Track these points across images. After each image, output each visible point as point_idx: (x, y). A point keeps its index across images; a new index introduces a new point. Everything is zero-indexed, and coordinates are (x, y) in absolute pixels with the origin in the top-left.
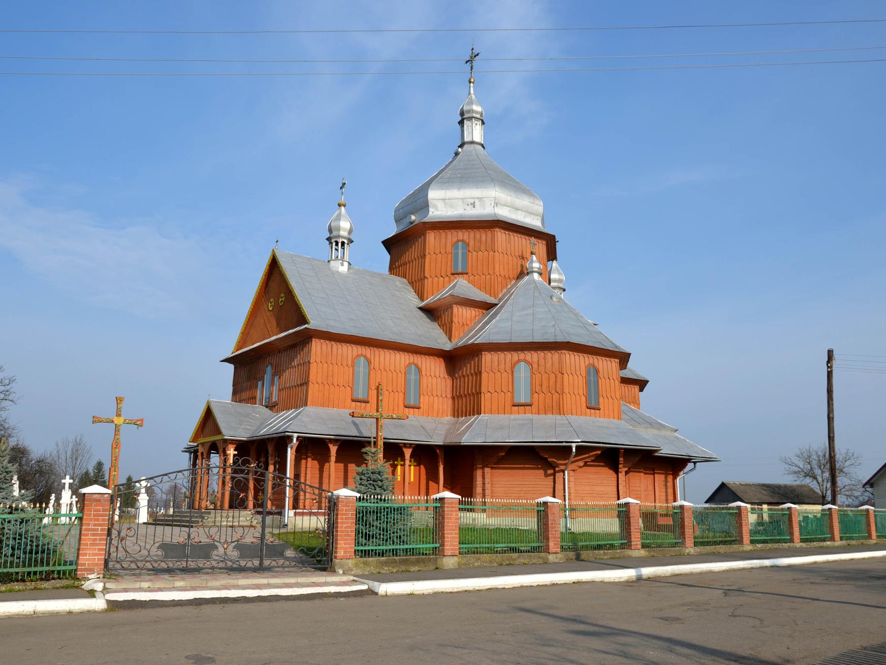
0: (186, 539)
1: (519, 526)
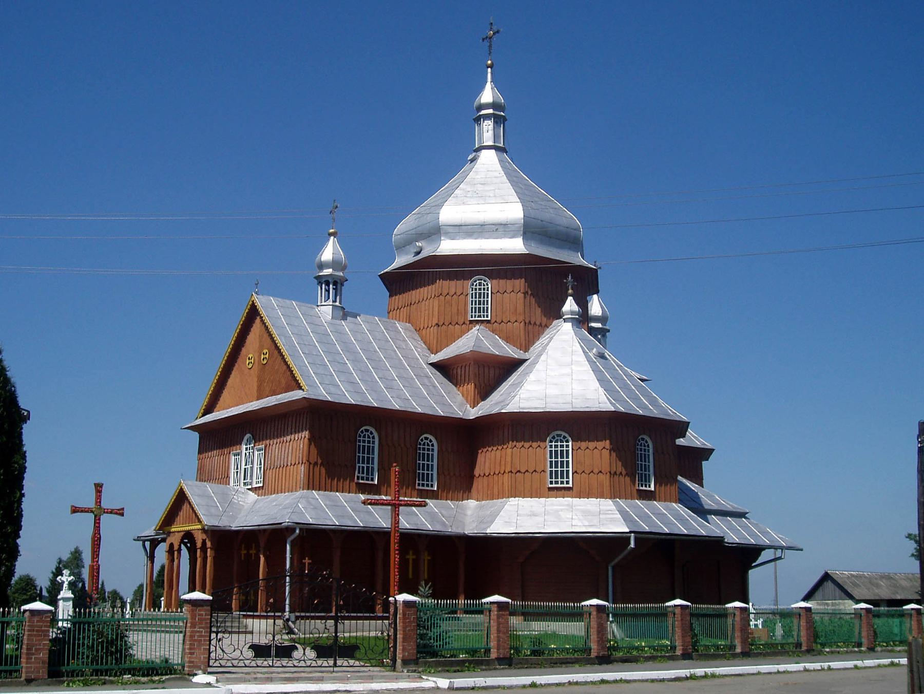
0: (271, 641)
1: (559, 632)
